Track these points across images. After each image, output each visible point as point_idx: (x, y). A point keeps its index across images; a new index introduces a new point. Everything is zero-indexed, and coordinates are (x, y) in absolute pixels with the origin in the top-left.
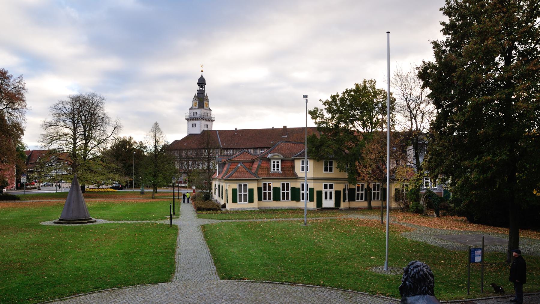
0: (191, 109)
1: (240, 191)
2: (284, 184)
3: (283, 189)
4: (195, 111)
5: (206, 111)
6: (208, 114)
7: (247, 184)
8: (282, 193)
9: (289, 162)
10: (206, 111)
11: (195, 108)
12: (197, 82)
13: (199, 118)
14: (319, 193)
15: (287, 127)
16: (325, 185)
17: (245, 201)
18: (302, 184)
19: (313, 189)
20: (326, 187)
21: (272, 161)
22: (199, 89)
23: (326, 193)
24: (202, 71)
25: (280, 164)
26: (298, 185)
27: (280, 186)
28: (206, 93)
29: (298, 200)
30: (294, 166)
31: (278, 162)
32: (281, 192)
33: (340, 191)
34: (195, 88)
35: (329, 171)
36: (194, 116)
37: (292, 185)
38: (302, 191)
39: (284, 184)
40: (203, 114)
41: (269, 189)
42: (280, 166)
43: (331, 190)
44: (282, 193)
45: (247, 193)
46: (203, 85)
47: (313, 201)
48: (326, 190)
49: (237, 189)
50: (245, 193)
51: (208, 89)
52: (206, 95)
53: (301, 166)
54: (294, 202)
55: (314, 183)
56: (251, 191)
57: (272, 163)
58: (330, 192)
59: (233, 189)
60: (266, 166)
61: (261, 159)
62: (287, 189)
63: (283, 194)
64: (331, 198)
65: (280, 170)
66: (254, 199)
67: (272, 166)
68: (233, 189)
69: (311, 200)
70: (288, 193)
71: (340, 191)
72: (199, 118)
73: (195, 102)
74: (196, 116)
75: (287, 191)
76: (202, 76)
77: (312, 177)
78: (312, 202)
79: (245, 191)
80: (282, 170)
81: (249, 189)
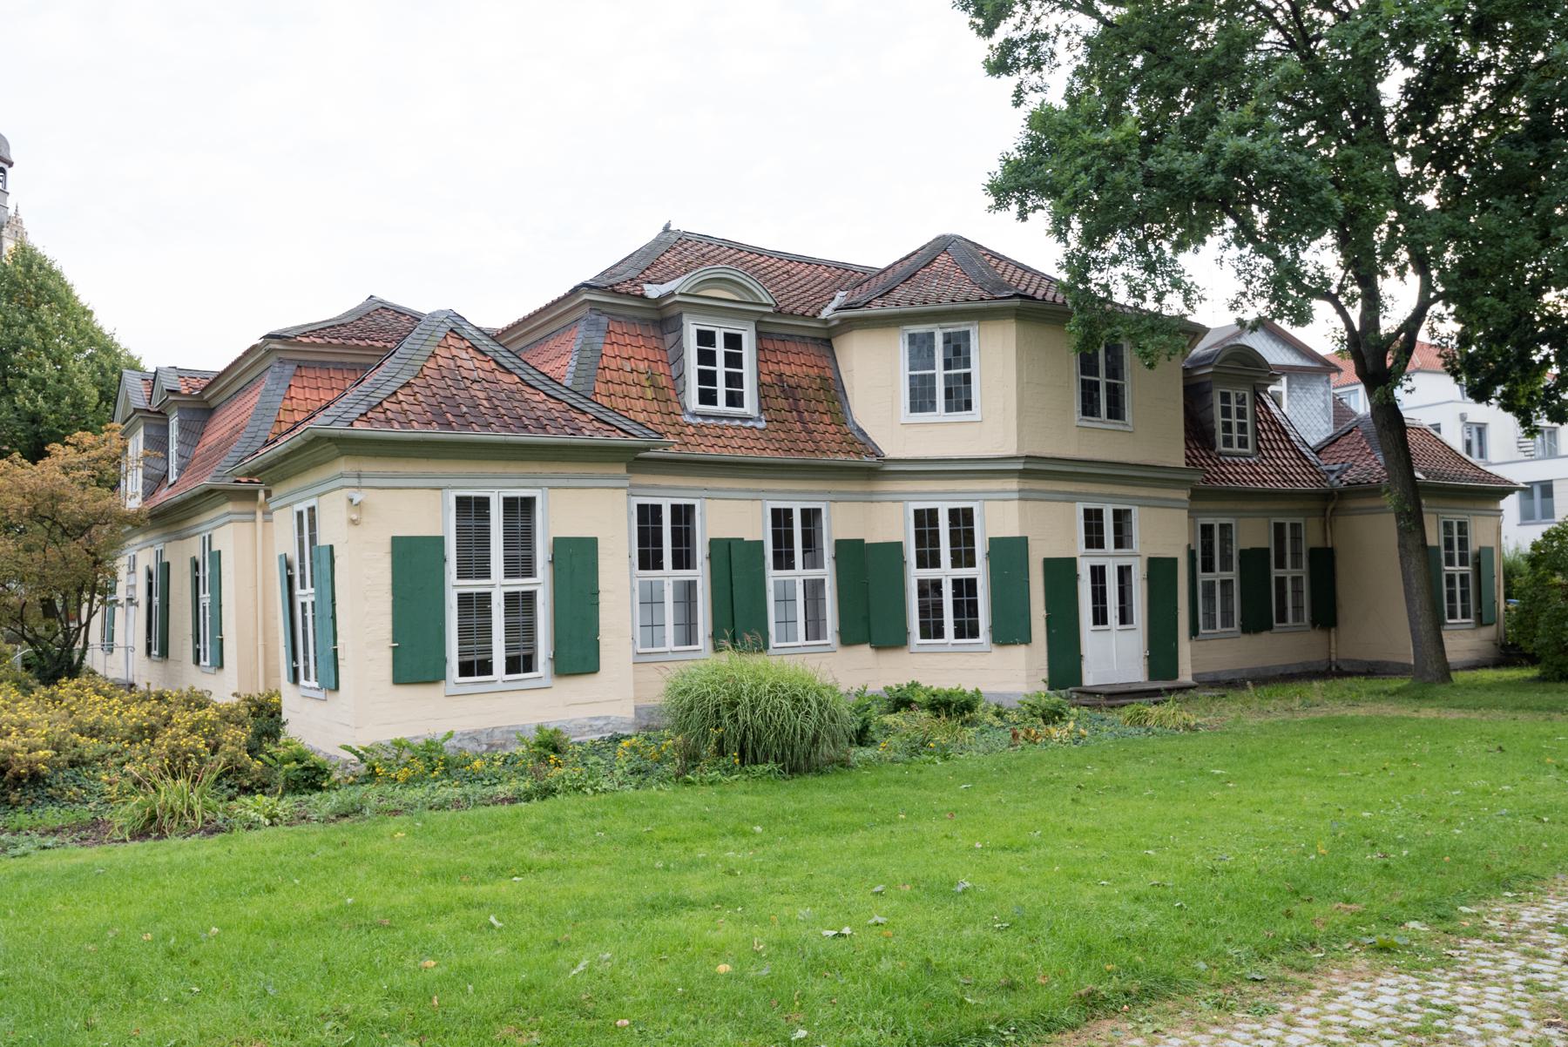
1: (474, 565)
2: (789, 512)
3: (928, 558)
9: (791, 346)
14: (1060, 572)
16: (1087, 512)
19: (1022, 543)
23: (1098, 574)
27: (762, 532)
29: (889, 638)
31: (733, 341)
32: (914, 575)
33: (1174, 561)
39: (789, 512)
41: (964, 557)
42: (748, 370)
45: (541, 583)
49: (439, 541)
50: (520, 585)
52: (11, 212)
54: (864, 652)
55: (1024, 496)
57: (691, 347)
59: (396, 541)
62: (964, 557)
63: (930, 590)
64: (1125, 618)
65: (750, 406)
67: (692, 367)
68: (396, 541)
69: (1010, 631)
70: (972, 584)
71: (1174, 561)
75: (964, 573)
77: (1011, 450)
78: (1018, 653)
79: (520, 564)
80: (762, 410)
81: (560, 545)
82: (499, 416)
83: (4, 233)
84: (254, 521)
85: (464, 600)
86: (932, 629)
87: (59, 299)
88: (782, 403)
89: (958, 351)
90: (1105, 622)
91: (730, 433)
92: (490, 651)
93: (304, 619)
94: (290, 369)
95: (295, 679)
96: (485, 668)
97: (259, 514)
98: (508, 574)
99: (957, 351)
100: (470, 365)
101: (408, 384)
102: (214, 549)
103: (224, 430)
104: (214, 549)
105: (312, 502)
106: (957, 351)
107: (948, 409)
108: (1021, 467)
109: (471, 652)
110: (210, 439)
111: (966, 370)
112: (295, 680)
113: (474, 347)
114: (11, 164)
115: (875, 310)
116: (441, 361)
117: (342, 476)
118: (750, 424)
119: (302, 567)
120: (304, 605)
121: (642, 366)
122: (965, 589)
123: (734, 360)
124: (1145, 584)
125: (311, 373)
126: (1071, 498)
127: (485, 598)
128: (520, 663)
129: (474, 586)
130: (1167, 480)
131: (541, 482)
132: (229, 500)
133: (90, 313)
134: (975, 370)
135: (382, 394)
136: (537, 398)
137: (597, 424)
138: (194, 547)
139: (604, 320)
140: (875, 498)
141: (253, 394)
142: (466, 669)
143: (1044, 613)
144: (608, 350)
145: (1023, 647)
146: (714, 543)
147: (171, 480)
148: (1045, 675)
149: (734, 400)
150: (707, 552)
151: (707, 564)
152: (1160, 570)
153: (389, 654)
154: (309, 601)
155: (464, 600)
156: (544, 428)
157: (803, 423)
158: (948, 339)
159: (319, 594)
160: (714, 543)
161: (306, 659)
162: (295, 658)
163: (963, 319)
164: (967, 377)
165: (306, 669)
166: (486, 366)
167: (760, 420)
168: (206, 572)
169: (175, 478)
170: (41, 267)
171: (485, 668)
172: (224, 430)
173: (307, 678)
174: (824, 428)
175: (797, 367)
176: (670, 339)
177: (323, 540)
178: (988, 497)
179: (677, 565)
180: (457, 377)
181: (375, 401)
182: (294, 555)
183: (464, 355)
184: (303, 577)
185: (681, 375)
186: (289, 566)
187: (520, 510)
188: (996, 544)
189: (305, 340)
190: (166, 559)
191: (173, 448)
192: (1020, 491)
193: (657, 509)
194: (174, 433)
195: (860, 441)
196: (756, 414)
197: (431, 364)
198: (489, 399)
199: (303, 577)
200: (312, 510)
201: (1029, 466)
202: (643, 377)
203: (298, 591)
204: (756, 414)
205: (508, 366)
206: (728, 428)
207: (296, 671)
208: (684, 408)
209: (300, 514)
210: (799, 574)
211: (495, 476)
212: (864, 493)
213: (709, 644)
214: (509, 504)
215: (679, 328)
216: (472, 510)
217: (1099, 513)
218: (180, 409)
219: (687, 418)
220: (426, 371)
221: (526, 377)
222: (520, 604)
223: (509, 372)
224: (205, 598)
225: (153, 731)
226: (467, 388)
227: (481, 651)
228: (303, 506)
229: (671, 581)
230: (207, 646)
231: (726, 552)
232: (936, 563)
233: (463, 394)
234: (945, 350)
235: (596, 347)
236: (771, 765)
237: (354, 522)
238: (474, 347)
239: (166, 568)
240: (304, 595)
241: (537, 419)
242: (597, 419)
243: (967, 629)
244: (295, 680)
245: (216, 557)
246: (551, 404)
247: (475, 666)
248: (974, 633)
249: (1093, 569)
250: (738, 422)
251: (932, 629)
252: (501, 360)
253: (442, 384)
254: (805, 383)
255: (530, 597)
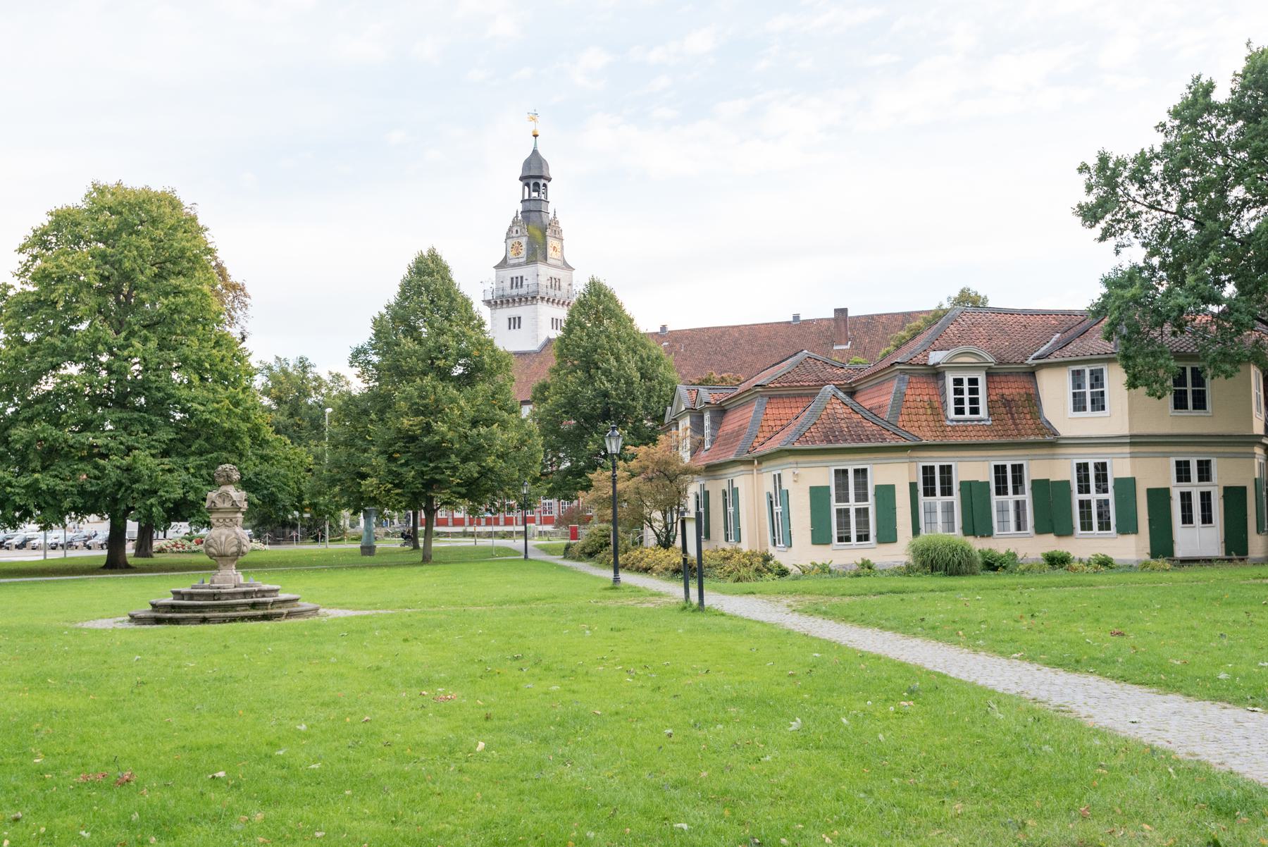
0: (503, 264)
1: (843, 497)
3: (1084, 489)
4: (517, 272)
5: (554, 273)
6: (562, 283)
7: (1024, 463)
8: (866, 500)
9: (1011, 379)
10: (554, 273)
11: (516, 261)
12: (519, 173)
13: (534, 298)
14: (1159, 498)
15: (850, 314)
16: (1178, 463)
17: (1104, 526)
18: (925, 468)
20: (1183, 472)
21: (950, 379)
22: (526, 197)
23: (1186, 497)
24: (536, 136)
25: (982, 386)
26: (1062, 469)
28: (551, 209)
30: (1037, 395)
31: (973, 382)
32: (1077, 497)
33: (1244, 488)
34: (513, 196)
35: (1195, 408)
36: (515, 292)
37: (1037, 468)
38: (1080, 492)
40: (543, 280)
43: (1205, 487)
44: (866, 500)
45: (871, 504)
46: (542, 182)
47: (1135, 530)
48: (1185, 487)
50: (862, 505)
51: (557, 199)
53: (1069, 391)
55: (1133, 456)
56: (886, 494)
58: (1202, 494)
59: (811, 488)
60: (926, 398)
61: (902, 371)
63: (1085, 505)
64: (1207, 519)
65: (983, 413)
66: (899, 528)
67: (951, 397)
68: (811, 488)
69: (1127, 526)
70: (1106, 502)
71: (1244, 488)
72: (534, 298)
73: (515, 240)
74: (522, 291)
76: (535, 152)
77: (1126, 432)
78: (1130, 539)
79: (861, 496)
80: (990, 414)
82: (851, 435)
83: (547, 233)
84: (753, 474)
85: (839, 511)
86: (1086, 526)
87: (616, 316)
88: (1003, 410)
89: (1097, 379)
90: (1191, 522)
91: (969, 429)
92: (850, 532)
93: (778, 520)
94: (766, 399)
95: (775, 545)
96: (848, 539)
97: (755, 471)
98: (856, 501)
99: (1097, 379)
100: (841, 411)
101: (815, 424)
102: (735, 486)
103: (735, 425)
104: (735, 486)
105: (779, 472)
106: (1097, 379)
107: (1093, 410)
108: (1128, 441)
109: (842, 533)
110: (726, 428)
111: (1102, 389)
112: (775, 545)
113: (843, 403)
114: (549, 180)
115: (1052, 359)
116: (828, 411)
117: (790, 463)
118: (983, 423)
119: (776, 498)
120: (777, 513)
121: (926, 398)
122: (1103, 504)
123: (974, 391)
124: (1222, 502)
125: (775, 401)
126: (1167, 455)
127: (847, 511)
128: (863, 537)
129: (843, 505)
130: (1239, 442)
131: (870, 462)
132: (742, 464)
133: (631, 321)
134: (1106, 389)
135: (804, 430)
136: (869, 425)
137: (893, 436)
138: (724, 484)
139: (907, 377)
140: (1055, 457)
141: (749, 410)
142: (840, 539)
143: (1147, 517)
144: (909, 392)
145: (1133, 536)
146: (962, 483)
147: (706, 447)
148: (1149, 550)
149: (974, 411)
150: (959, 487)
151: (959, 493)
152: (1234, 496)
153: (810, 533)
154: (779, 511)
155: (839, 511)
156: (869, 439)
157: (1013, 418)
158: (1092, 372)
159: (783, 509)
160: (962, 483)
161: (779, 535)
162: (774, 535)
163: (1099, 362)
164: (1102, 393)
165: (779, 540)
166: (847, 411)
167: (988, 420)
168: (730, 498)
169: (709, 446)
170: (605, 295)
171: (848, 539)
172: (735, 425)
173: (779, 543)
174: (1027, 422)
175: (1012, 389)
176: (940, 383)
177: (784, 488)
178: (1114, 456)
179: (943, 494)
180: (834, 418)
181: (802, 433)
182: (772, 492)
183: (838, 407)
184: (776, 501)
185: (945, 401)
186: (771, 497)
187: (861, 473)
188: (1118, 481)
189: (772, 386)
190: (706, 489)
191: (707, 431)
192: (1130, 453)
193: (932, 468)
194: (707, 423)
195: (1049, 429)
196: (986, 417)
197: (824, 413)
198: (847, 427)
199: (776, 501)
200: (779, 475)
201: (1133, 440)
202: (926, 404)
203: (775, 507)
204: (986, 417)
205: (857, 410)
206: (970, 426)
207: (775, 540)
208: (947, 418)
209: (775, 475)
210: (1010, 498)
211: (850, 460)
212: (1049, 455)
213: (961, 532)
214: (856, 471)
215: (944, 378)
216: (841, 474)
217: (1187, 463)
218: (711, 411)
219: (948, 423)
220: (822, 416)
221: (864, 415)
222: (862, 513)
223: (857, 413)
224: (731, 509)
225: (570, 690)
226: (839, 423)
227: (846, 533)
228: (776, 473)
229: (940, 502)
230: (732, 532)
231: (970, 489)
232: (1088, 491)
233: (837, 426)
234: (1091, 378)
235: (902, 391)
236: (942, 572)
237: (795, 481)
238: (843, 403)
239: (707, 494)
240: (778, 509)
241: (867, 436)
242: (894, 434)
243: (1104, 526)
244: (775, 545)
245: (735, 491)
246: (875, 427)
247: (845, 538)
248: (1108, 528)
249: (1202, 494)
250: (976, 423)
251: (1086, 526)
252: (854, 408)
253: (828, 422)
254: (1017, 398)
255: (866, 510)
